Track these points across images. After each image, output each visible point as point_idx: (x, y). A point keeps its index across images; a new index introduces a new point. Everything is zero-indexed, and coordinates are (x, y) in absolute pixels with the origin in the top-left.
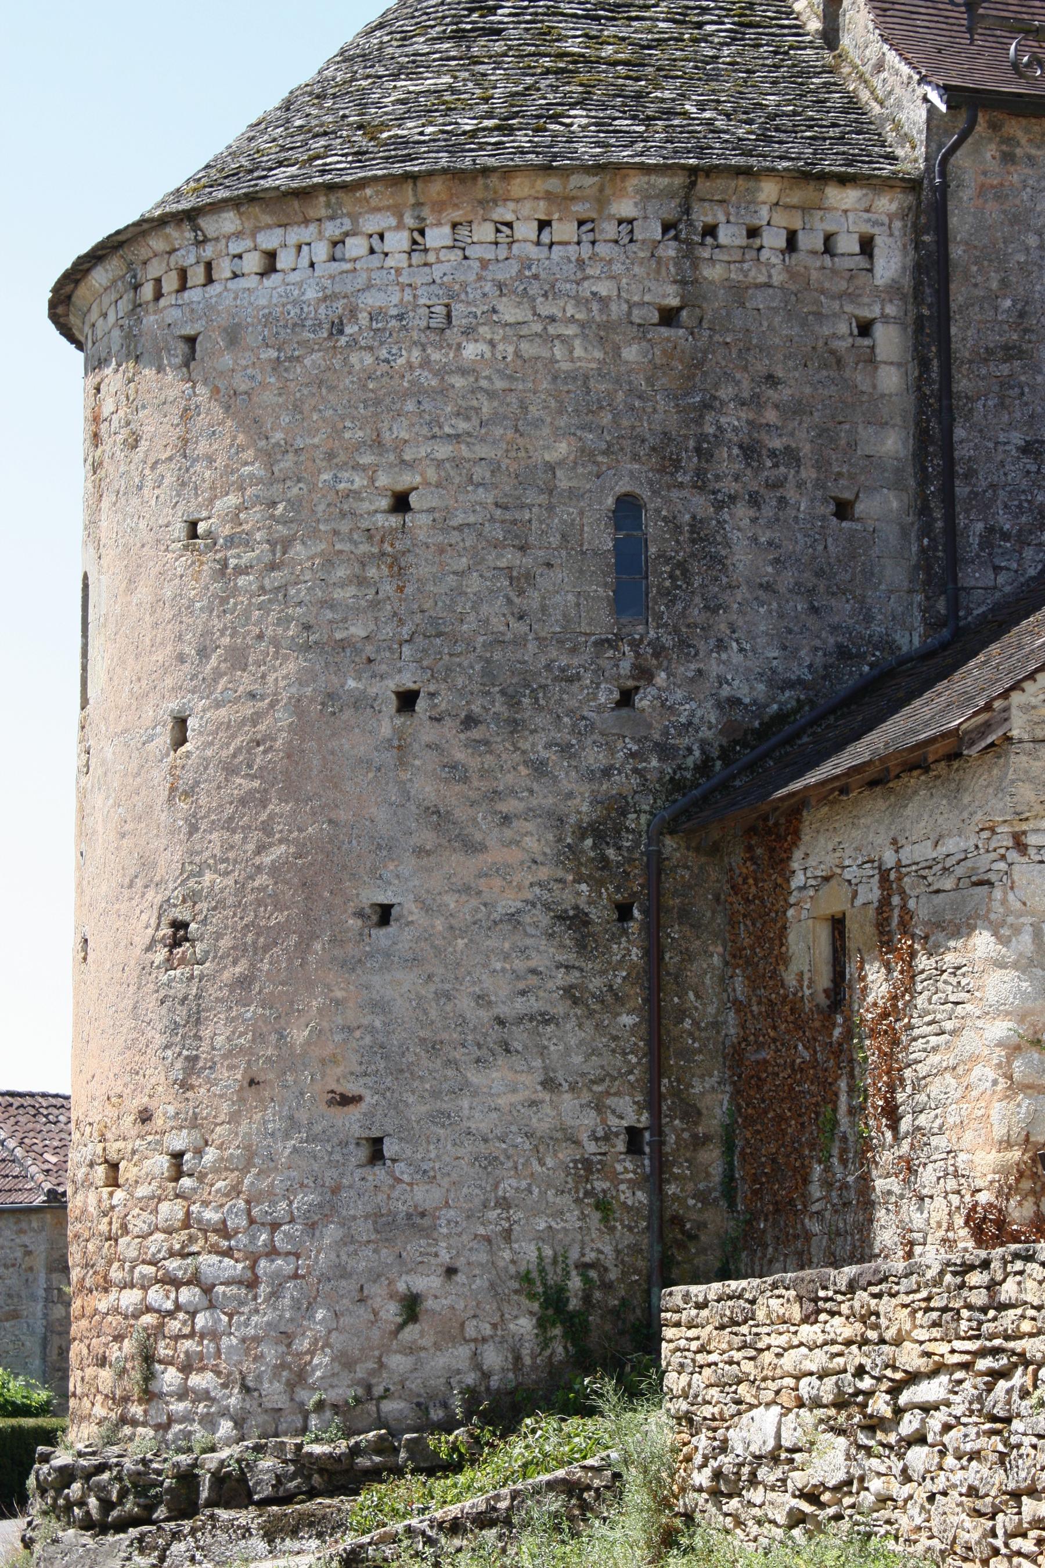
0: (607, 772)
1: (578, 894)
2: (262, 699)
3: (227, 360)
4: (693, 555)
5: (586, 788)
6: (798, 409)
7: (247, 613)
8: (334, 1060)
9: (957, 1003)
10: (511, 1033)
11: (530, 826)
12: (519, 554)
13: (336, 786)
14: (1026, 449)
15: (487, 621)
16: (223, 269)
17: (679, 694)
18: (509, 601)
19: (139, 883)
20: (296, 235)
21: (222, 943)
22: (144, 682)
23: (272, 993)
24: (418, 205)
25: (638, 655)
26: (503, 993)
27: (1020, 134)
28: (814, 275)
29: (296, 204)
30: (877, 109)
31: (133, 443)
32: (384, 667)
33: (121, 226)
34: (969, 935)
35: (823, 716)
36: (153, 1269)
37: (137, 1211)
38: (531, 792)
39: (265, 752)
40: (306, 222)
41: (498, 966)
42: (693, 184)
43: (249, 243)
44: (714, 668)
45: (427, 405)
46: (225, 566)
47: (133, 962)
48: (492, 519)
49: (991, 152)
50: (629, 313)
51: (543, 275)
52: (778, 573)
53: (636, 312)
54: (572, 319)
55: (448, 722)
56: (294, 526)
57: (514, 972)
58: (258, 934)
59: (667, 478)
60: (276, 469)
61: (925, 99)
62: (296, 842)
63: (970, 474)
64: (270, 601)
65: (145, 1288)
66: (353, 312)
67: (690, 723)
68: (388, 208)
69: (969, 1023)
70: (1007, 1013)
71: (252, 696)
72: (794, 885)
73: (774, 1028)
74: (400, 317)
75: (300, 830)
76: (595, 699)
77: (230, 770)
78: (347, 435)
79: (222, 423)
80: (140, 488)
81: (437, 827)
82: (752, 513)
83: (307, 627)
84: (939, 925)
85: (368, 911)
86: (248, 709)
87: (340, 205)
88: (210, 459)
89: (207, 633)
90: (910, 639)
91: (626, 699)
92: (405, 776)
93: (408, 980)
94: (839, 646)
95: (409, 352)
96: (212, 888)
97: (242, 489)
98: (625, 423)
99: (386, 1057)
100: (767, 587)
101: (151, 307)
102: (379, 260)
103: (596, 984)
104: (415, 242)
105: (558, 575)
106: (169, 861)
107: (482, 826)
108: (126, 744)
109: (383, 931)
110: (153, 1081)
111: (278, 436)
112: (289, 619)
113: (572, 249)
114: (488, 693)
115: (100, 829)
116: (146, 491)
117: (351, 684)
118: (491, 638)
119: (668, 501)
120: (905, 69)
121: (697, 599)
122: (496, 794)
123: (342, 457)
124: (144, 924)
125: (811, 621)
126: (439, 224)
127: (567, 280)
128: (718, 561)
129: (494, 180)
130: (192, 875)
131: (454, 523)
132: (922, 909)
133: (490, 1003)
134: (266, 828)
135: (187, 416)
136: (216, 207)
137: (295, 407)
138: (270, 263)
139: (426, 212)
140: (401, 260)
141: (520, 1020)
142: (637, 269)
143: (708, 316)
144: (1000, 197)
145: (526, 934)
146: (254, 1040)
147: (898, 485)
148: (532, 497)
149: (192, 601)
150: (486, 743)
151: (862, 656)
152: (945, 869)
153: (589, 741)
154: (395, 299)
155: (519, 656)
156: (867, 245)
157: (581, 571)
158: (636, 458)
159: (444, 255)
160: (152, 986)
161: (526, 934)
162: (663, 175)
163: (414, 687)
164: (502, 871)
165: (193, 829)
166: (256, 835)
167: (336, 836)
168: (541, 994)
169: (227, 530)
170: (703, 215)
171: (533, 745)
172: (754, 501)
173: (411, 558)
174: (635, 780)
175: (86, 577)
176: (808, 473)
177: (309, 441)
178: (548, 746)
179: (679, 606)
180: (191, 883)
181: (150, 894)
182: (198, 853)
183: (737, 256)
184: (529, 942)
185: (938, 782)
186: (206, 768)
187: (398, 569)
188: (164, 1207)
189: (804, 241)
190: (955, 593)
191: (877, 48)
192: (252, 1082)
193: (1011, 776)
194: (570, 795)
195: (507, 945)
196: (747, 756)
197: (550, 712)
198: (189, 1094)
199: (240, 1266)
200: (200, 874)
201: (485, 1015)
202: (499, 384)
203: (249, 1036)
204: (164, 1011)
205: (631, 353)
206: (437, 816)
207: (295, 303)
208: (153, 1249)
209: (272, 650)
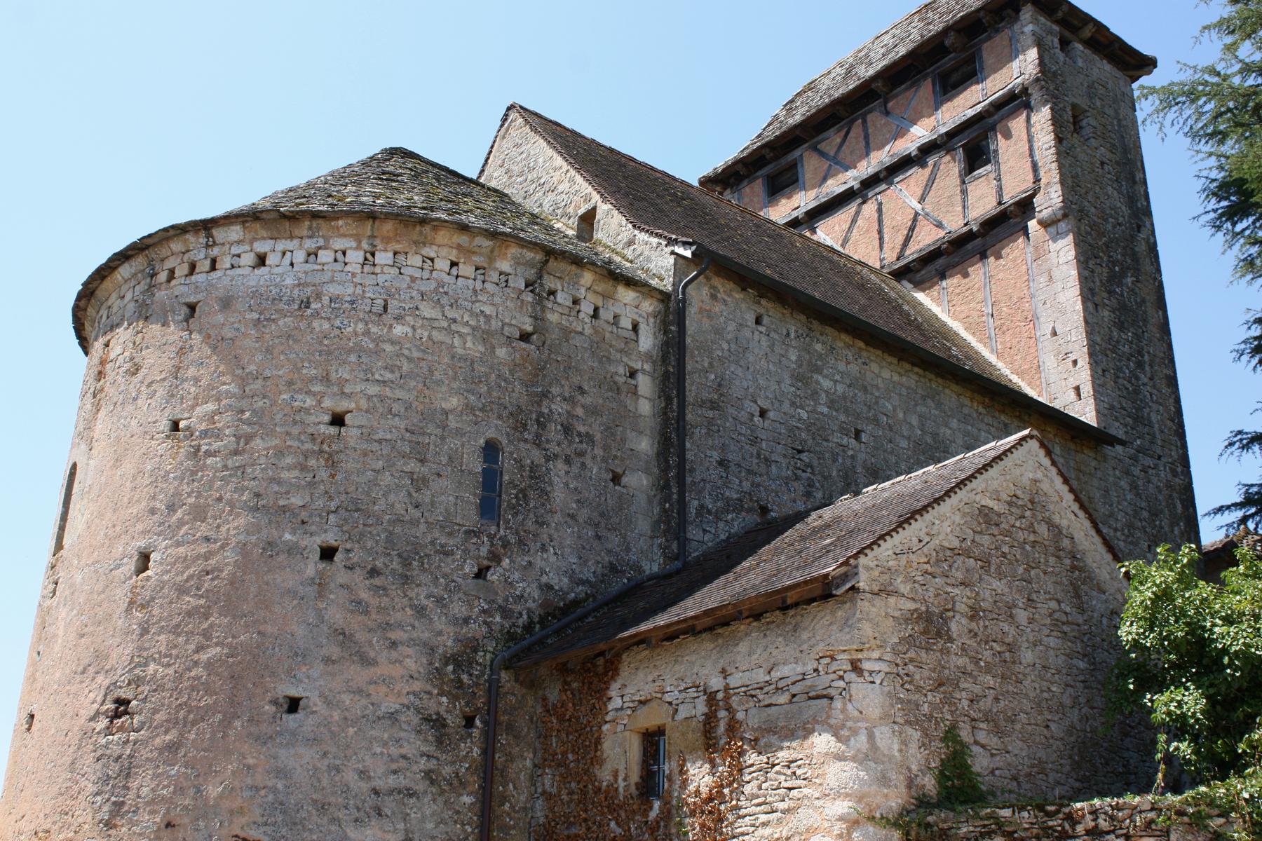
0: (466, 621)
1: (440, 704)
2: (216, 541)
3: (220, 318)
4: (530, 486)
5: (451, 630)
6: (593, 411)
7: (211, 483)
8: (241, 812)
9: (790, 789)
10: (383, 801)
11: (410, 651)
12: (419, 464)
13: (267, 607)
14: (721, 463)
15: (393, 506)
16: (225, 262)
17: (517, 576)
18: (410, 495)
19: (91, 670)
20: (281, 245)
21: (157, 717)
22: (118, 528)
23: (195, 757)
24: (373, 237)
25: (492, 545)
26: (380, 771)
28: (607, 335)
29: (287, 224)
30: (628, 265)
32: (314, 527)
33: (153, 231)
34: (805, 737)
35: (601, 607)
38: (413, 627)
39: (212, 579)
40: (292, 238)
41: (378, 750)
42: (547, 261)
44: (539, 563)
45: (364, 359)
46: (199, 450)
47: (76, 729)
48: (403, 439)
49: (705, 291)
50: (502, 328)
51: (451, 293)
52: (579, 509)
53: (506, 328)
55: (358, 571)
56: (257, 427)
57: (389, 756)
58: (189, 712)
60: (247, 389)
61: (673, 253)
62: (230, 646)
63: (692, 470)
64: (230, 475)
66: (318, 296)
67: (522, 596)
68: (351, 236)
69: (806, 802)
70: (847, 795)
71: (207, 539)
72: (610, 707)
73: (586, 811)
74: (352, 302)
75: (234, 637)
76: (462, 569)
77: (182, 590)
78: (304, 371)
79: (210, 357)
80: (135, 399)
81: (342, 644)
82: (566, 468)
83: (258, 495)
84: (771, 731)
85: (281, 700)
86: (203, 549)
87: (318, 229)
88: (196, 380)
89: (177, 494)
90: (652, 566)
91: (481, 574)
92: (321, 605)
93: (308, 755)
94: (611, 563)
95: (356, 324)
96: (155, 675)
97: (219, 400)
98: (495, 394)
99: (284, 812)
100: (572, 517)
101: (163, 287)
103: (447, 770)
104: (366, 259)
105: (443, 482)
106: (121, 655)
107: (376, 647)
108: (96, 572)
109: (292, 716)
110: (80, 820)
111: (253, 368)
112: (244, 489)
114: (389, 554)
116: (140, 401)
117: (288, 536)
118: (394, 517)
121: (531, 515)
122: (388, 626)
123: (299, 385)
125: (596, 543)
126: (385, 250)
127: (466, 300)
129: (427, 229)
130: (139, 665)
131: (376, 437)
132: (750, 717)
133: (369, 777)
134: (206, 634)
135: (181, 352)
137: (267, 350)
138: (261, 260)
139: (377, 242)
140: (358, 269)
141: (391, 792)
142: (509, 303)
143: (549, 342)
144: (710, 317)
145: (401, 729)
146: (174, 792)
147: (647, 471)
148: (431, 429)
149: (168, 473)
150: (384, 589)
151: (623, 572)
152: (777, 689)
153: (456, 598)
154: (350, 291)
155: (413, 532)
156: (635, 328)
157: (460, 483)
158: (500, 417)
159: (386, 269)
160: (91, 747)
161: (401, 729)
162: (530, 250)
164: (386, 681)
165: (145, 631)
166: (198, 639)
167: (263, 644)
168: (408, 774)
170: (550, 283)
171: (418, 594)
172: (568, 461)
173: (342, 456)
174: (484, 629)
175: (74, 466)
176: (598, 451)
177: (275, 372)
178: (428, 597)
179: (520, 518)
180: (137, 671)
181: (100, 679)
182: (146, 649)
183: (567, 311)
184: (403, 734)
185: (772, 626)
186: (162, 589)
187: (332, 463)
190: (683, 542)
191: (627, 231)
192: (168, 825)
193: (858, 616)
194: (440, 633)
195: (386, 735)
196: (556, 625)
197: (432, 574)
198: (112, 832)
200: (146, 665)
201: (365, 786)
202: (416, 354)
203: (171, 789)
204: (99, 766)
206: (343, 636)
207: (276, 286)
209: (227, 509)
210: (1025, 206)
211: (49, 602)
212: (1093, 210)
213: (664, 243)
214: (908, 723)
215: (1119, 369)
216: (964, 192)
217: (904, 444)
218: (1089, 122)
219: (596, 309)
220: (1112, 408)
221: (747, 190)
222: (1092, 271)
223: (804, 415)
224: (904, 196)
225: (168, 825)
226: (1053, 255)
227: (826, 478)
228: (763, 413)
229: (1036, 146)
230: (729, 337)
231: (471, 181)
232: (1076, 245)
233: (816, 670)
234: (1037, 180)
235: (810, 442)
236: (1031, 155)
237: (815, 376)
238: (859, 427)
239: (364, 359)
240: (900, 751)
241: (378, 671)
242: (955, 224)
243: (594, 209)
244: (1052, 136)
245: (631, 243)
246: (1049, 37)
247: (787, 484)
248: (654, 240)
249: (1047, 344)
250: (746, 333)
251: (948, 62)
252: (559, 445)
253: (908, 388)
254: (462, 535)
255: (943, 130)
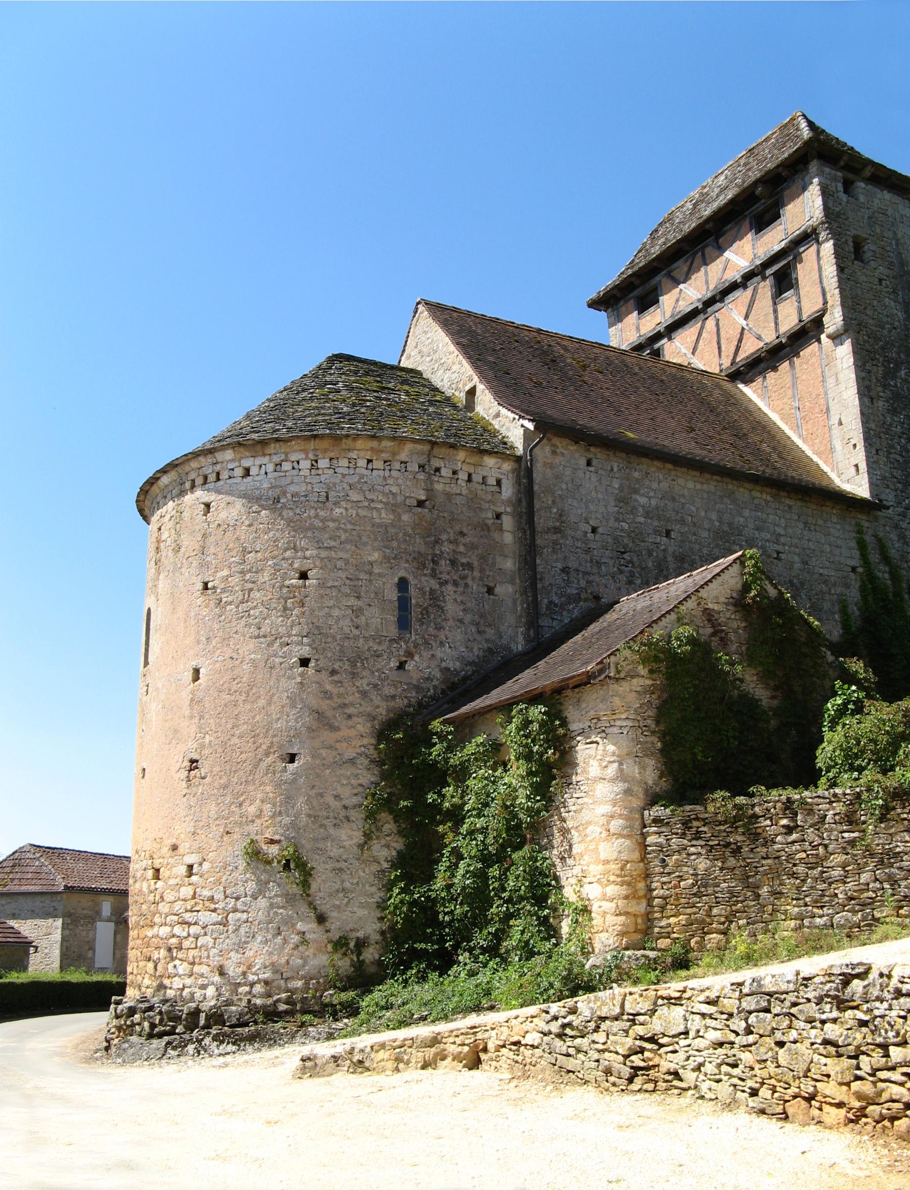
0: (393, 697)
4: (430, 605)
5: (384, 704)
6: (472, 547)
11: (360, 720)
16: (224, 475)
18: (352, 620)
20: (258, 461)
27: (558, 443)
28: (479, 492)
31: (177, 549)
36: (177, 917)
37: (169, 891)
38: (361, 705)
40: (264, 455)
41: (345, 782)
43: (237, 464)
44: (439, 653)
49: (547, 449)
50: (405, 501)
53: (408, 500)
54: (381, 501)
55: (323, 672)
59: (420, 571)
61: (522, 426)
65: (172, 926)
66: (284, 493)
68: (302, 450)
74: (306, 496)
82: (454, 589)
86: (230, 664)
91: (401, 666)
94: (489, 648)
100: (461, 621)
102: (299, 469)
104: (312, 465)
107: (339, 720)
110: (179, 831)
113: (381, 473)
115: (154, 719)
119: (420, 581)
120: (511, 415)
121: (432, 624)
124: (178, 761)
125: (478, 637)
126: (324, 458)
128: (441, 608)
135: (204, 536)
136: (223, 448)
138: (247, 472)
139: (318, 453)
140: (307, 473)
142: (408, 483)
147: (512, 582)
148: (362, 576)
150: (341, 682)
151: (498, 653)
156: (499, 483)
158: (407, 561)
159: (326, 471)
162: (420, 444)
163: (308, 656)
164: (347, 740)
169: (222, 586)
171: (362, 684)
172: (455, 584)
176: (477, 574)
178: (368, 685)
179: (424, 627)
184: (359, 771)
188: (183, 889)
189: (475, 478)
190: (538, 628)
191: (495, 407)
194: (378, 707)
197: (370, 670)
199: (220, 917)
202: (349, 527)
205: (405, 517)
208: (177, 908)
210: (817, 323)
211: (145, 698)
212: (871, 321)
213: (517, 417)
214: (646, 755)
215: (892, 447)
216: (775, 311)
217: (705, 534)
218: (869, 248)
219: (470, 475)
220: (884, 478)
221: (623, 308)
222: (869, 372)
223: (625, 526)
224: (732, 313)
225: (228, 833)
226: (839, 361)
227: (643, 569)
228: (594, 530)
229: (824, 274)
230: (567, 479)
231: (392, 367)
232: (855, 353)
233: (590, 727)
234: (825, 303)
235: (631, 545)
236: (821, 282)
237: (634, 496)
238: (669, 528)
239: (317, 534)
240: (640, 773)
241: (341, 734)
242: (770, 337)
243: (475, 387)
244: (835, 267)
245: (497, 415)
246: (834, 184)
247: (613, 577)
248: (513, 415)
249: (836, 431)
250: (580, 474)
251: (758, 207)
252: (448, 574)
253: (708, 493)
254: (387, 643)
255: (758, 262)
